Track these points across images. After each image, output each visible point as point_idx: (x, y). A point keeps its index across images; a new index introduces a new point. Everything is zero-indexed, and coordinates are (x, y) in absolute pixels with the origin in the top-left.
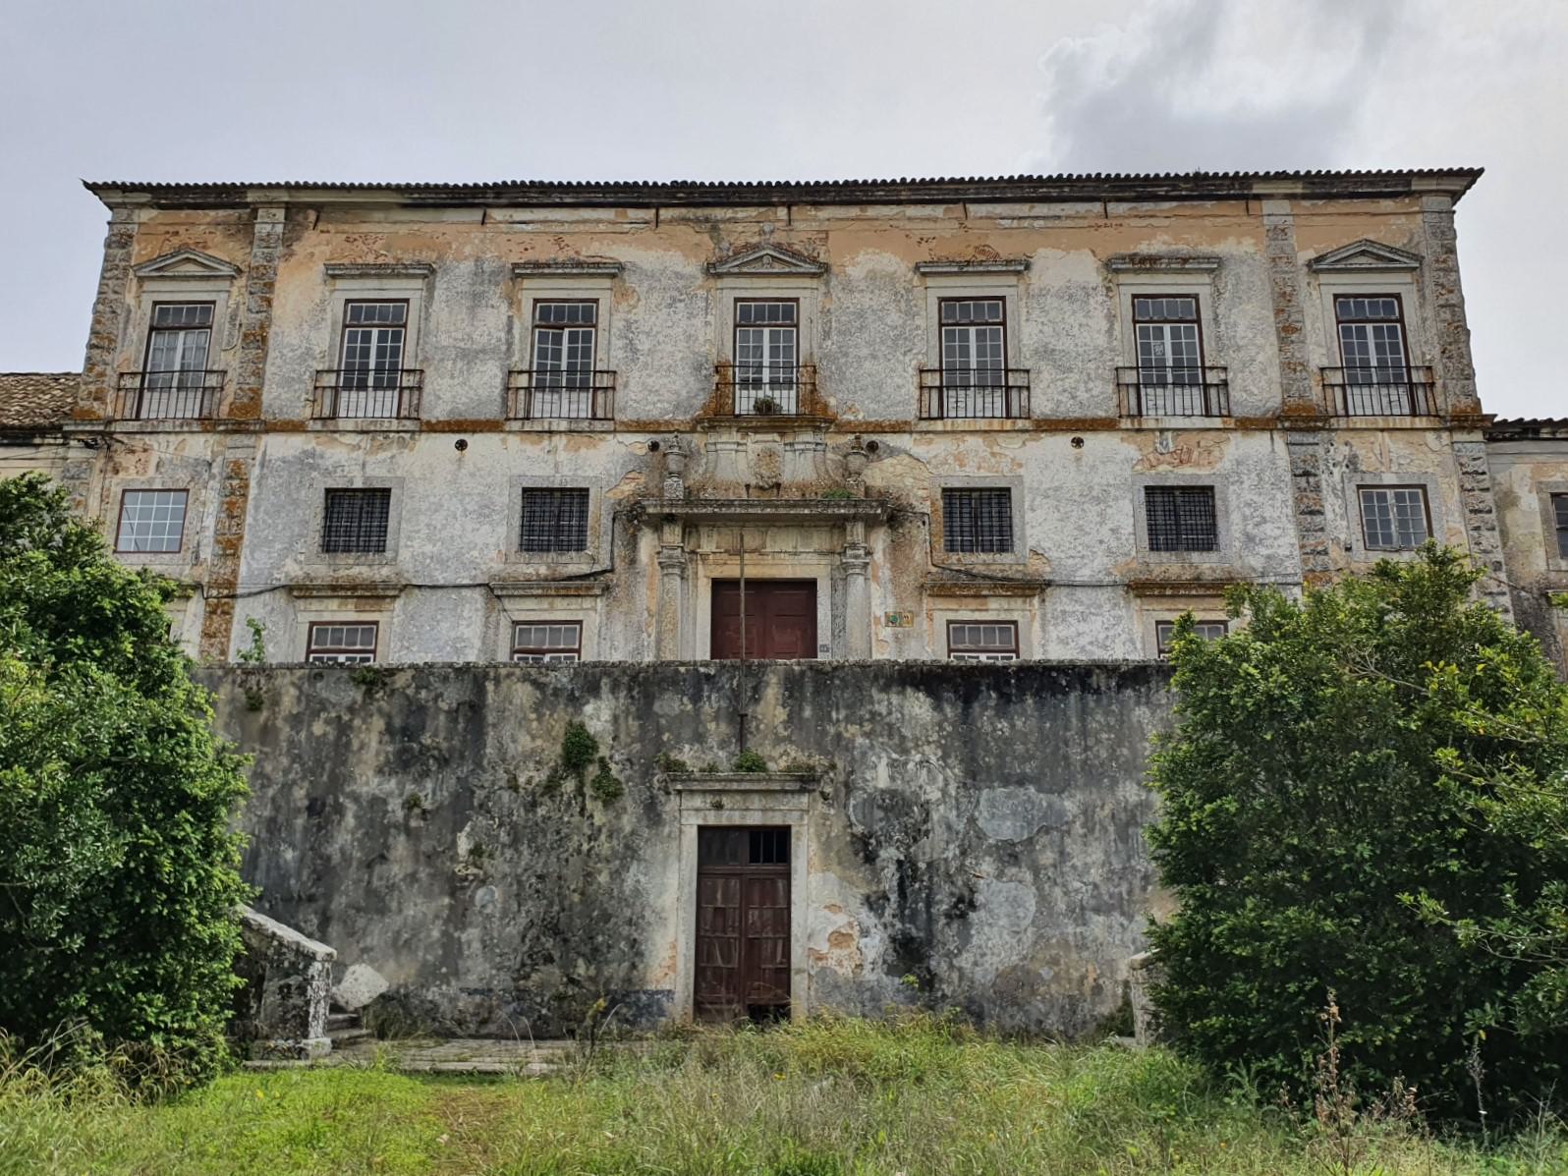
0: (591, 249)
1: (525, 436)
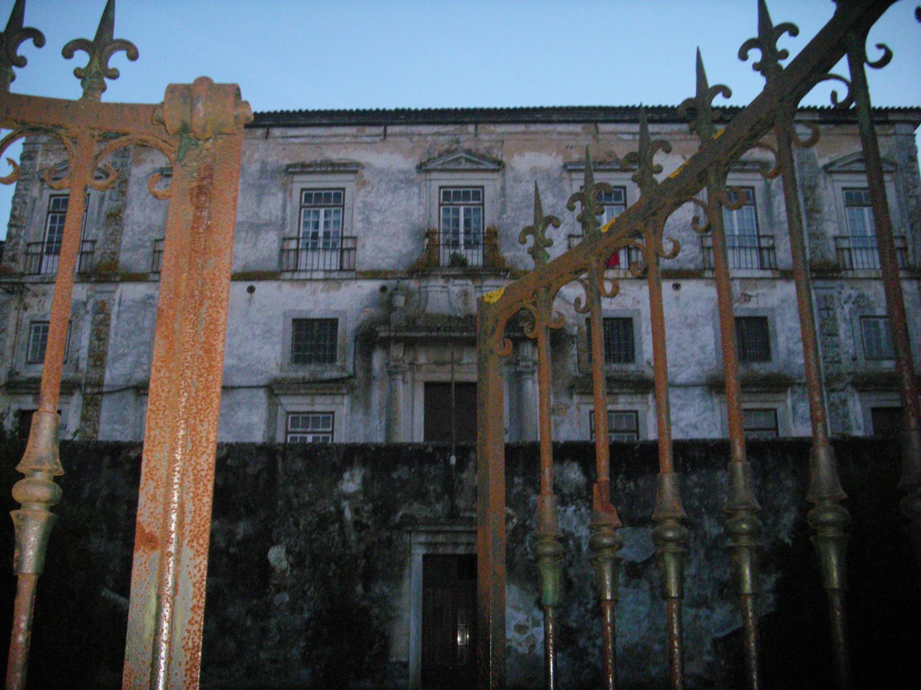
0: (335, 155)
1: (295, 283)
